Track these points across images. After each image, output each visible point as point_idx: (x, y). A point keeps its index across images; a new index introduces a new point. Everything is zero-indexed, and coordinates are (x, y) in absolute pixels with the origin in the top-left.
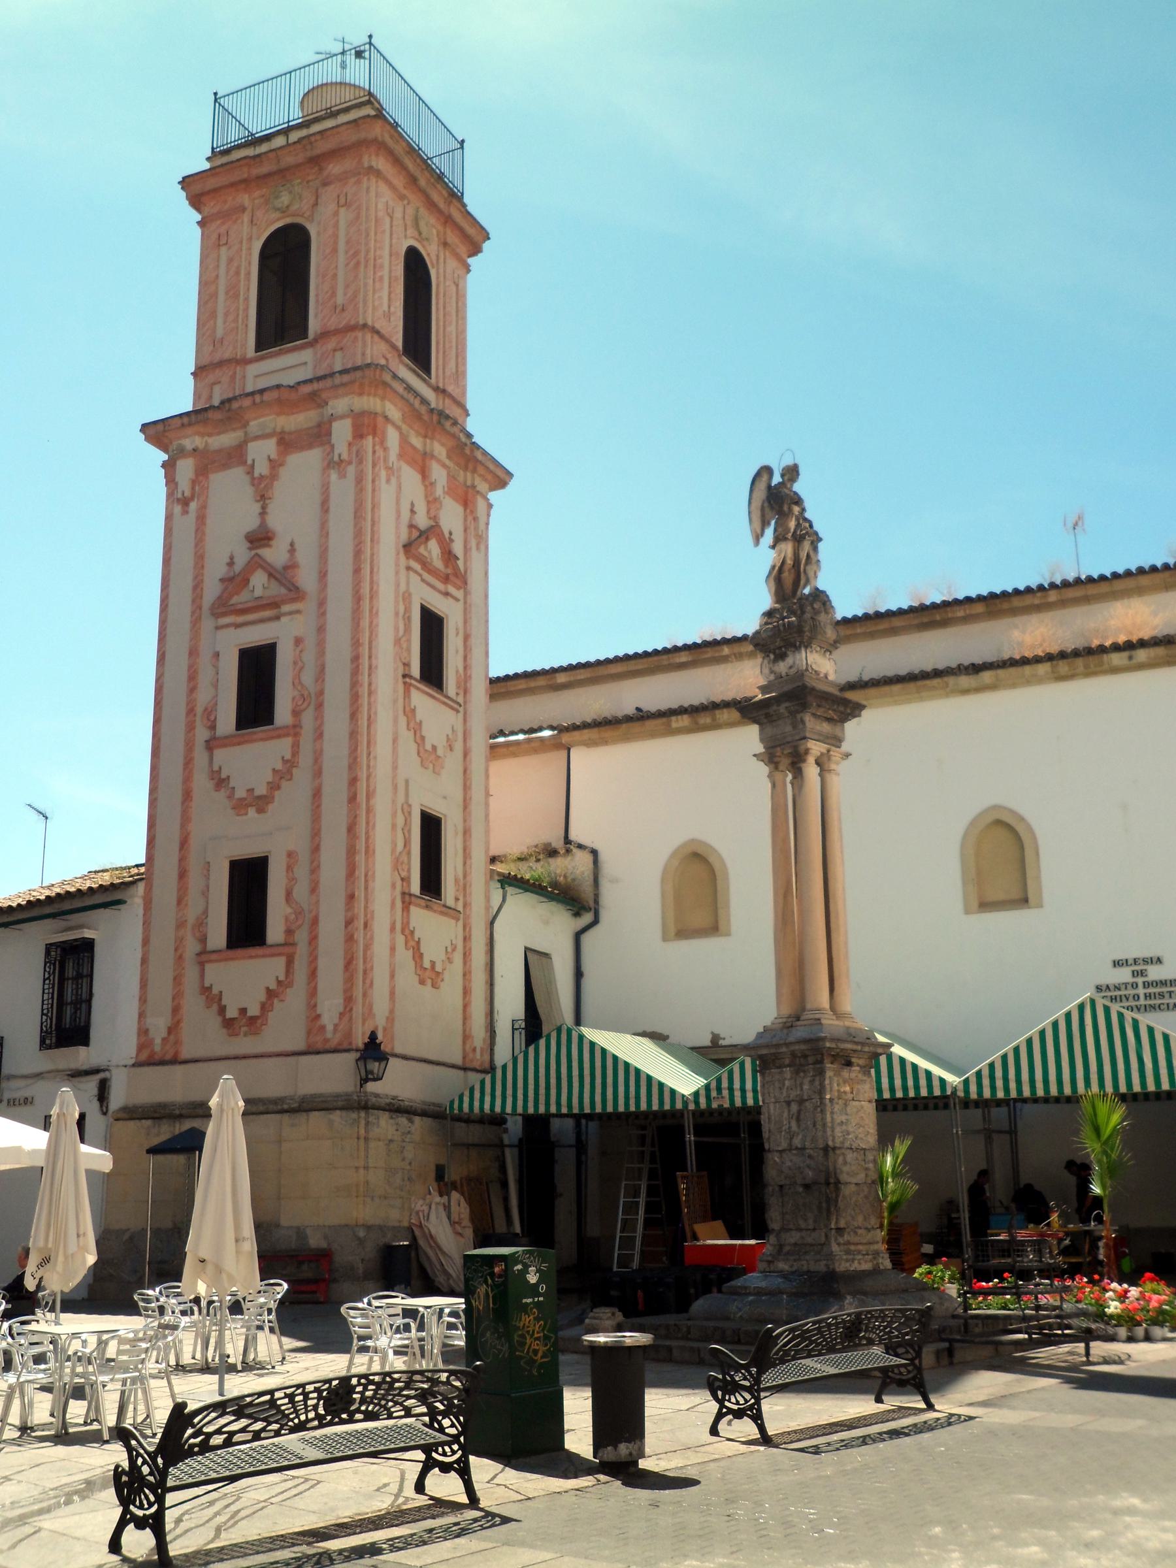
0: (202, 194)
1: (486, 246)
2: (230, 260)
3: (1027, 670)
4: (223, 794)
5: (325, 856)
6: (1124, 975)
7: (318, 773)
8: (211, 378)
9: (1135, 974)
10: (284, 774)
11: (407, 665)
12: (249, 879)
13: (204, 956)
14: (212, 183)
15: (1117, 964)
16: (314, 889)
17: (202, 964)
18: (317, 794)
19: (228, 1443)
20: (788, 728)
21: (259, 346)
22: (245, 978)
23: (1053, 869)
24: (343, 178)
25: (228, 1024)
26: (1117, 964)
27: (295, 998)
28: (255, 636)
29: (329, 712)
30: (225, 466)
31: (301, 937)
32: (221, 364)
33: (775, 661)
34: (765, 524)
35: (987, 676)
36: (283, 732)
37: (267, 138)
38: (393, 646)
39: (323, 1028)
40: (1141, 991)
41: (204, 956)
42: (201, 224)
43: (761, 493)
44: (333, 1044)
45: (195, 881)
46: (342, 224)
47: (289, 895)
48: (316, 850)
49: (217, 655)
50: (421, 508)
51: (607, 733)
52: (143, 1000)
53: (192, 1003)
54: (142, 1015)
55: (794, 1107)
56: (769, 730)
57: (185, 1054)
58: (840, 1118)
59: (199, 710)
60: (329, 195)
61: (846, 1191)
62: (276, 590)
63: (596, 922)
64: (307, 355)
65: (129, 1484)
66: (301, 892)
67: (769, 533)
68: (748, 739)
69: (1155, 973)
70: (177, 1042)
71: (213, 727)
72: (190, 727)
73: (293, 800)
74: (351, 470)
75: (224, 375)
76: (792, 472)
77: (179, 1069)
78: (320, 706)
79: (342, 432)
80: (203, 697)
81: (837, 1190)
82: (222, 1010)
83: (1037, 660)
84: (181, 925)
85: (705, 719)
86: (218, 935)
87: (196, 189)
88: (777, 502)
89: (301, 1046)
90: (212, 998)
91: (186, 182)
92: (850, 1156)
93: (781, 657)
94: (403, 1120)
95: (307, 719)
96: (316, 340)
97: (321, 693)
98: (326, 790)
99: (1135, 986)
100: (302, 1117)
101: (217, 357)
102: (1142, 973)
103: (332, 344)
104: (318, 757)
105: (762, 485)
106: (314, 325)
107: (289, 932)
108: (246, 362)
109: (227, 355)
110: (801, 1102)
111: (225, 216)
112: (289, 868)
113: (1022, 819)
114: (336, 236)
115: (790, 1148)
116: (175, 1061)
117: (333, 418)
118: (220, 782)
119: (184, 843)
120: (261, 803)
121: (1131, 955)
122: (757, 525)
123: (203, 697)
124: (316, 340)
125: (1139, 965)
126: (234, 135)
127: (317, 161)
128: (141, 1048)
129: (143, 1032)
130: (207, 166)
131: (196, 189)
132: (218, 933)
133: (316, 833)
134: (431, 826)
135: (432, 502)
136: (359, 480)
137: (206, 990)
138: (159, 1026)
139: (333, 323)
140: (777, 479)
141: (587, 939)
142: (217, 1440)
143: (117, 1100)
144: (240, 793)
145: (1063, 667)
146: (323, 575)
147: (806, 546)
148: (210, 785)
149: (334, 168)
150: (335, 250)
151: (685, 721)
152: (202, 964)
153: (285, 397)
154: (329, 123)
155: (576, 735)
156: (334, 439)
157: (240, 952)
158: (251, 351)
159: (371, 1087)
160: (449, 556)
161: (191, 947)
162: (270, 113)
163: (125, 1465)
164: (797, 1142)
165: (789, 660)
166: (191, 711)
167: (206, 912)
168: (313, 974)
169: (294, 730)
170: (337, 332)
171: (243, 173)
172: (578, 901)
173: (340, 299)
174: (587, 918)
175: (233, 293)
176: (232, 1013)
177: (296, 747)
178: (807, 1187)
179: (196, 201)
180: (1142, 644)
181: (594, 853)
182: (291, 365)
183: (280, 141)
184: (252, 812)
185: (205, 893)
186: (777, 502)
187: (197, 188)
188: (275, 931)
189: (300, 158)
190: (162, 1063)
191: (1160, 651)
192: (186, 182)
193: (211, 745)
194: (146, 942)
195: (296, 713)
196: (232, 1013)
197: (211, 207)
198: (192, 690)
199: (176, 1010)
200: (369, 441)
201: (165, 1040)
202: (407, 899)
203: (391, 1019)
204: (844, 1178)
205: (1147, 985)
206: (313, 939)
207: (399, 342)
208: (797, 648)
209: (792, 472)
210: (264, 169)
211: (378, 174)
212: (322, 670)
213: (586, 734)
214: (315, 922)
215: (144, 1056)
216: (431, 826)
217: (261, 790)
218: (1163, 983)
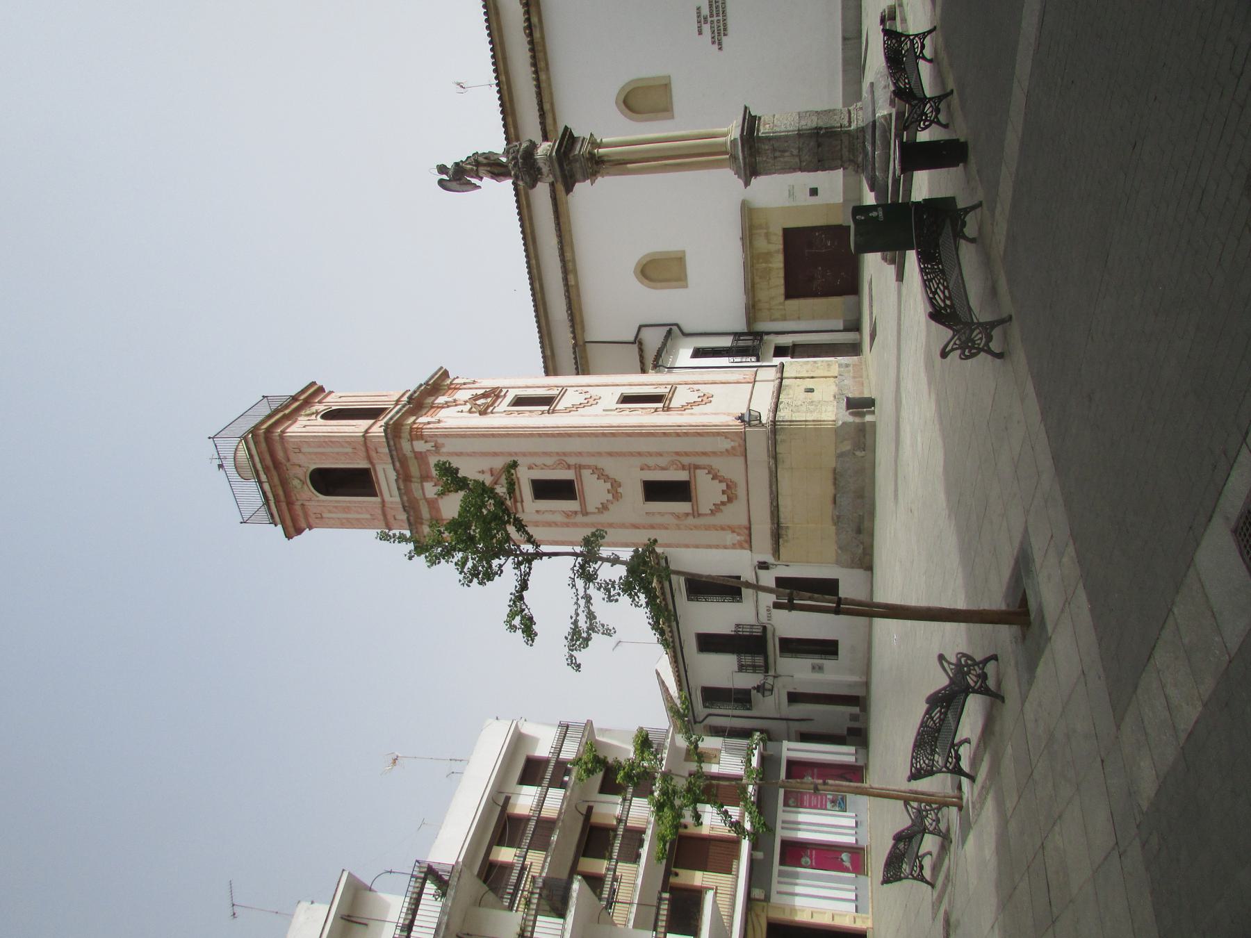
0: (294, 526)
1: (319, 383)
2: (330, 512)
3: (543, 85)
4: (610, 506)
5: (644, 449)
6: (706, 28)
7: (600, 454)
8: (391, 520)
9: (706, 22)
10: (601, 474)
11: (543, 412)
12: (655, 491)
13: (696, 514)
14: (289, 522)
15: (700, 33)
16: (660, 454)
17: (699, 515)
18: (610, 454)
19: (950, 298)
20: (578, 165)
21: (375, 495)
22: (707, 491)
23: (648, 69)
24: (285, 450)
25: (730, 500)
26: (700, 33)
27: (716, 463)
28: (526, 491)
29: (568, 449)
30: (438, 510)
31: (686, 460)
32: (384, 515)
33: (541, 174)
34: (469, 183)
35: (547, 107)
36: (580, 476)
37: (264, 493)
38: (532, 419)
39: (733, 448)
40: (715, 19)
41: (696, 514)
42: (310, 528)
43: (454, 185)
44: (742, 442)
45: (658, 520)
46: (311, 450)
47: (663, 469)
48: (640, 454)
49: (537, 512)
50: (459, 408)
51: (578, 319)
52: (717, 547)
53: (719, 519)
54: (725, 547)
55: (777, 154)
56: (579, 176)
57: (746, 523)
58: (783, 128)
59: (566, 520)
60: (294, 458)
61: (821, 124)
62: (503, 480)
63: (677, 325)
64: (379, 468)
65: (970, 349)
66: (662, 461)
67: (474, 181)
68: (582, 189)
69: (705, 11)
70: (739, 527)
71: (576, 513)
72: (575, 525)
73: (612, 467)
74: (440, 441)
75: (390, 514)
76: (442, 169)
77: (753, 527)
78: (564, 454)
79: (420, 446)
80: (559, 518)
81: (821, 128)
82: (723, 503)
83: (538, 79)
84: (678, 527)
85: (570, 265)
86: (683, 507)
87: (293, 530)
88: (458, 177)
89: (742, 459)
90: (717, 509)
91: (289, 536)
92: (803, 123)
93: (539, 169)
94: (781, 406)
95: (572, 461)
96: (371, 463)
97: (557, 454)
98: (608, 449)
99: (712, 22)
100: (779, 456)
101: (381, 517)
102: (705, 18)
103: (373, 454)
104: (592, 455)
105: (449, 184)
106: (363, 464)
107: (683, 468)
108: (383, 501)
109: (380, 512)
110: (774, 150)
111: (306, 516)
112: (649, 468)
113: (623, 88)
114: (316, 453)
115: (799, 156)
116: (750, 529)
117: (413, 451)
118: (604, 508)
119: (636, 527)
120: (615, 486)
121: (696, 25)
122: (469, 187)
123: (559, 518)
124: (371, 463)
125: (701, 20)
126: (263, 513)
127: (277, 465)
128: (742, 548)
129: (734, 546)
130: (280, 526)
131: (293, 530)
132: (682, 507)
133: (631, 454)
134: (626, 399)
135: (456, 403)
136: (446, 436)
137: (713, 512)
138: (730, 538)
139: (362, 454)
140: (445, 177)
141: (687, 329)
142: (948, 302)
143: (769, 559)
144: (610, 497)
145: (542, 65)
146: (495, 454)
147: (481, 159)
148: (606, 513)
149: (280, 455)
150: (323, 454)
151: (571, 277)
152: (699, 515)
153: (404, 477)
154: (257, 459)
155: (579, 337)
156: (424, 450)
157: (693, 494)
158: (378, 499)
159: (764, 420)
160: (484, 396)
161: (691, 521)
162: (251, 494)
163: (959, 352)
164: (795, 152)
165: (541, 164)
166: (567, 525)
167: (673, 514)
168: (705, 454)
169: (579, 468)
170: (367, 451)
171: (284, 505)
172: (673, 332)
173: (349, 450)
174: (675, 328)
175: (347, 509)
176: (725, 498)
177: (589, 467)
178: (819, 145)
179: (299, 531)
180: (528, 20)
181: (640, 327)
182: (386, 475)
183: (267, 487)
184: (620, 490)
185: (661, 514)
186: (458, 177)
187: (291, 530)
188: (682, 476)
189: (274, 473)
190: (750, 535)
191: (533, 10)
192: (289, 536)
193: (585, 513)
194: (687, 546)
195: (569, 467)
196: (725, 498)
197: (303, 524)
198: (556, 524)
199: (723, 529)
200: (426, 432)
201: (739, 534)
202: (667, 409)
203: (729, 414)
204: (814, 125)
205: (712, 16)
206: (686, 454)
207: (372, 421)
208: (535, 160)
209: (442, 169)
210: (281, 492)
211: (283, 432)
212: (545, 454)
213: (578, 331)
214: (677, 453)
215: (746, 545)
216: (626, 399)
217: (608, 485)
218: (711, 6)
